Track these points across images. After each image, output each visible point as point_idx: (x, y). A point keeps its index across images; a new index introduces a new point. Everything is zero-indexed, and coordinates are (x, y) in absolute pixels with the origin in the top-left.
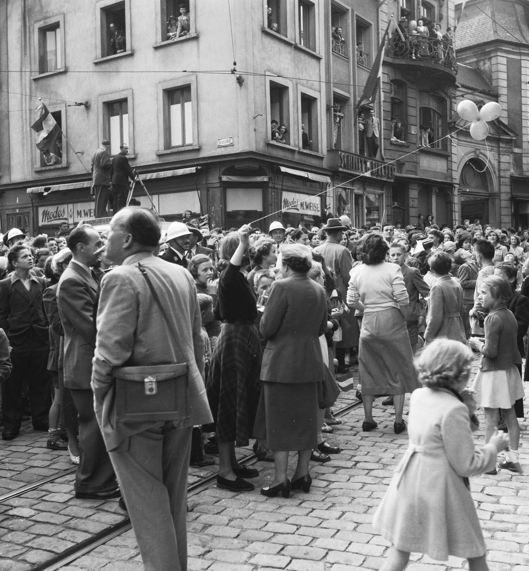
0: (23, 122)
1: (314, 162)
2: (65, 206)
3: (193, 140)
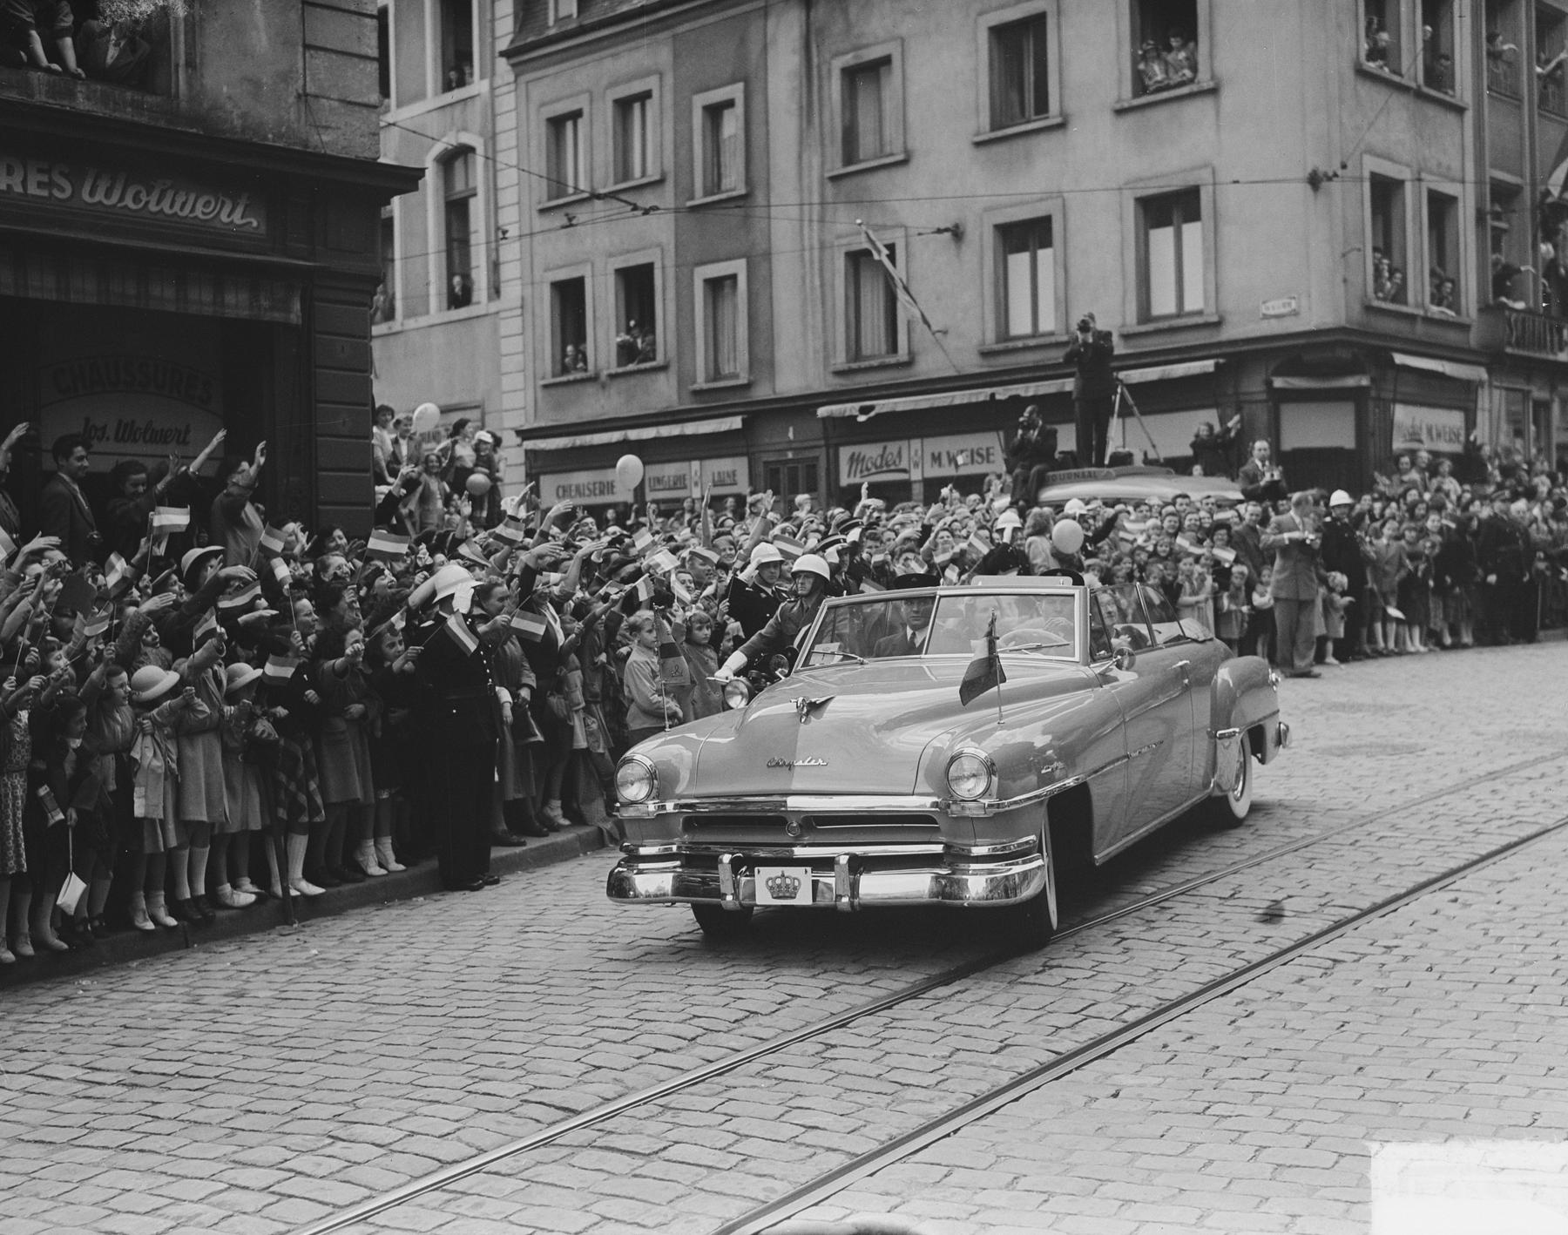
0: (804, 267)
1: (1453, 337)
2: (904, 444)
3: (1206, 299)
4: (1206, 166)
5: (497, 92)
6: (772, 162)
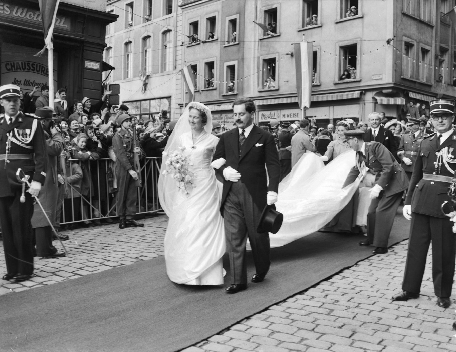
2: (276, 111)
4: (359, 38)
5: (178, 15)
6: (245, 35)
